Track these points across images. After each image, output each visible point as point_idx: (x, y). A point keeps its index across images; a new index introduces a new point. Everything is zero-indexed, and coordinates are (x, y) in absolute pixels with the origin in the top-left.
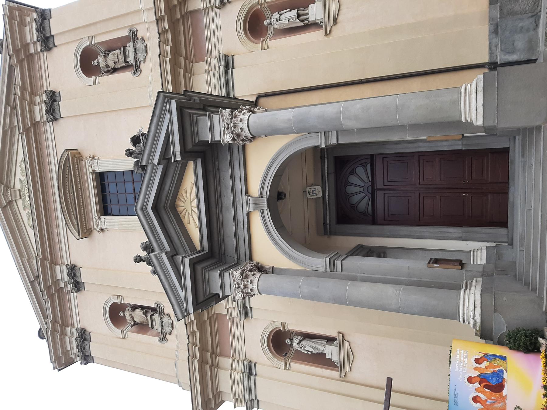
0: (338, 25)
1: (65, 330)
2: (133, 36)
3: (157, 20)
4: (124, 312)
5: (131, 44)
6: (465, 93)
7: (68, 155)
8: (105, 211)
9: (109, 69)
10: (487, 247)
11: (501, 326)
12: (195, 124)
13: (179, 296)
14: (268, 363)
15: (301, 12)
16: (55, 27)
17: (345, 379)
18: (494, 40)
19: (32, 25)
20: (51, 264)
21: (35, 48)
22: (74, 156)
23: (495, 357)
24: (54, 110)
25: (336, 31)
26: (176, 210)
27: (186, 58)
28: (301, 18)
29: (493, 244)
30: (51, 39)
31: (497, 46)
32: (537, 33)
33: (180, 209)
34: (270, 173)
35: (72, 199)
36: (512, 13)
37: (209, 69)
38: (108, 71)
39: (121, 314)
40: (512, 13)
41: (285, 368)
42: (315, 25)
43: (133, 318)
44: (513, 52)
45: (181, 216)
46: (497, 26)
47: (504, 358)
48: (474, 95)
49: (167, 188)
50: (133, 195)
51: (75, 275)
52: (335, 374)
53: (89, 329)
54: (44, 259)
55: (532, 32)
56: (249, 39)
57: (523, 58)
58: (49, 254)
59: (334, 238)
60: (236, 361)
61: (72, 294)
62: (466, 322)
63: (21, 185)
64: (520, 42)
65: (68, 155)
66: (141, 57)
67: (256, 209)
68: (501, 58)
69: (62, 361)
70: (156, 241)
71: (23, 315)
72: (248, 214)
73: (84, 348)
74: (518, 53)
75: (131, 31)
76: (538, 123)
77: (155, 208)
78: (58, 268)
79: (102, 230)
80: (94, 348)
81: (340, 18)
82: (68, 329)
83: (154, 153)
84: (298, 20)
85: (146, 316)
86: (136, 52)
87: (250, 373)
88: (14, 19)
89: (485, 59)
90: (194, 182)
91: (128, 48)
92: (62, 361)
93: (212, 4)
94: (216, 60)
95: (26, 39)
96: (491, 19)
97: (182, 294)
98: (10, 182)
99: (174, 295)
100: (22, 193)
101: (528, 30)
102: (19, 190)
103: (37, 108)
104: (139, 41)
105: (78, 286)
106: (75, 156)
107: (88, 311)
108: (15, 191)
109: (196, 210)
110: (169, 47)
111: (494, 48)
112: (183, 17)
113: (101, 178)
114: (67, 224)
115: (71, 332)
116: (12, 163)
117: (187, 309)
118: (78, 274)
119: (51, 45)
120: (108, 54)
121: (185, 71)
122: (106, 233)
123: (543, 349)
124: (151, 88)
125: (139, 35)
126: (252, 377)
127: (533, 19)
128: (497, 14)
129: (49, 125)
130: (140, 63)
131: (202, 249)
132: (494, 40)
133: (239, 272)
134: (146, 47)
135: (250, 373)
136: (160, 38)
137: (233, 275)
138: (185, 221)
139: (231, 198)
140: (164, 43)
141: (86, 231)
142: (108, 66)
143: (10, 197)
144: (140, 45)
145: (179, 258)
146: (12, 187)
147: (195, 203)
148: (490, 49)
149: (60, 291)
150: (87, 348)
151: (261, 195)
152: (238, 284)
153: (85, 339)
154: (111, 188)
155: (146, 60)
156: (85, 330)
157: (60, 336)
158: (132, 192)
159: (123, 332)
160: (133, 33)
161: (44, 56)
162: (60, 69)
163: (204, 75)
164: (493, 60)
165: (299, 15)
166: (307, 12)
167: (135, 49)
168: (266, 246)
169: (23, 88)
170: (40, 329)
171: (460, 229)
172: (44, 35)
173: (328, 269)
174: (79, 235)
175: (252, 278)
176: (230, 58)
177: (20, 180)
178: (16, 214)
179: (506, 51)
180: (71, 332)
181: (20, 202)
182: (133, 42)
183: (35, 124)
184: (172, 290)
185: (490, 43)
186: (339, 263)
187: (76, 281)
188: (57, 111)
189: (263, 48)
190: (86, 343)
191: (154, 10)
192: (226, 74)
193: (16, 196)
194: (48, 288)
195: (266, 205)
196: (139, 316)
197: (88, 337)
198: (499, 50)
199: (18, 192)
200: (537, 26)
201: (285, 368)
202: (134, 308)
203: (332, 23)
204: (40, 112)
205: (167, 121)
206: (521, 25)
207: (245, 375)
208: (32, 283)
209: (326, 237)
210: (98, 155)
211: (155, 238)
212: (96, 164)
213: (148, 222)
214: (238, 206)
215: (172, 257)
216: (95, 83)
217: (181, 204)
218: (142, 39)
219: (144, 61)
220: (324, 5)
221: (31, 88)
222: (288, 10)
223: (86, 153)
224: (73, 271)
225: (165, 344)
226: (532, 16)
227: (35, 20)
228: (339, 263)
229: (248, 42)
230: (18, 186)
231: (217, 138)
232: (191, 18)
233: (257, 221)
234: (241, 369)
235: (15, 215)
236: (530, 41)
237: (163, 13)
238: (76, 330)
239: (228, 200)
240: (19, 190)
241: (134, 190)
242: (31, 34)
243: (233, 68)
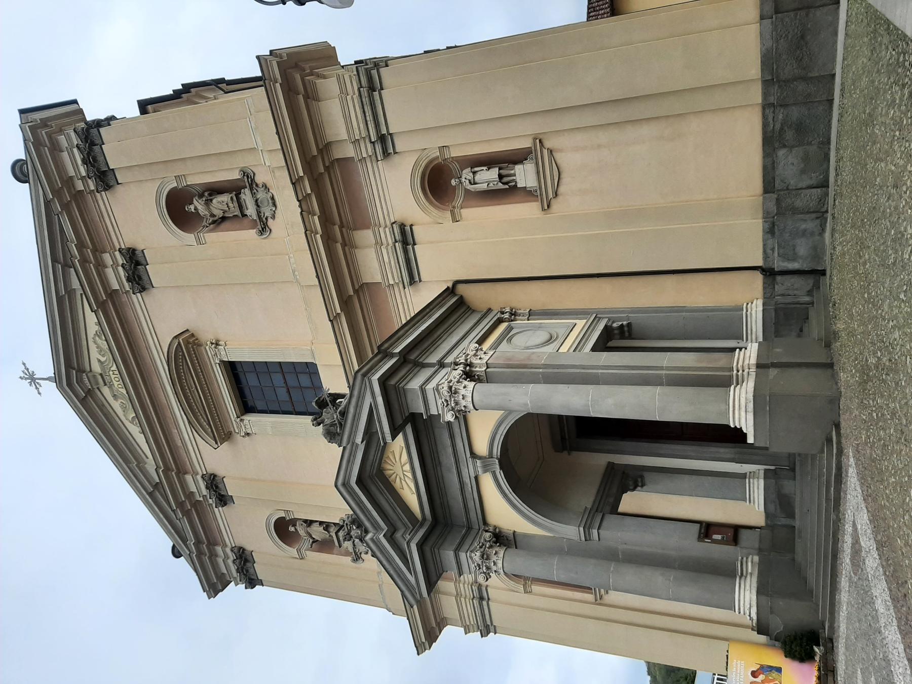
0: (560, 198)
1: (214, 550)
2: (248, 181)
3: (293, 184)
4: (294, 525)
5: (247, 191)
6: (734, 407)
7: (179, 343)
8: (246, 408)
9: (216, 218)
10: (766, 471)
11: (777, 624)
12: (403, 396)
13: (408, 580)
14: (502, 585)
15: (503, 172)
16: (114, 153)
17: (602, 602)
18: (769, 246)
19: (72, 152)
20: (178, 474)
21: (86, 184)
22: (187, 343)
23: (771, 668)
24: (140, 278)
25: (556, 205)
26: (383, 474)
27: (341, 226)
28: (505, 180)
29: (773, 468)
30: (110, 176)
31: (773, 249)
32: (824, 239)
33: (388, 473)
34: (500, 432)
35: (201, 408)
36: (795, 211)
37: (379, 243)
38: (214, 222)
39: (292, 529)
40: (795, 211)
41: (526, 592)
42: (528, 194)
43: (311, 536)
44: (794, 258)
45: (390, 479)
46: (773, 224)
47: (779, 670)
48: (743, 414)
49: (371, 457)
50: (285, 390)
51: (217, 487)
52: (590, 597)
53: (249, 547)
54: (167, 470)
55: (817, 238)
56: (431, 203)
57: (806, 266)
58: (174, 464)
59: (575, 453)
60: (461, 585)
61: (216, 510)
62: (742, 612)
63: (103, 368)
64: (803, 248)
65: (179, 343)
66: (267, 211)
67: (485, 472)
68: (779, 264)
69: (214, 585)
70: (369, 520)
71: (143, 532)
72: (476, 478)
73: (247, 571)
74: (801, 261)
75: (245, 173)
76: (813, 452)
77: (359, 481)
78: (189, 478)
79: (248, 434)
80: (260, 570)
81: (562, 189)
82: (219, 549)
83: (356, 432)
84: (500, 184)
85: (329, 532)
86: (258, 206)
87: (481, 598)
88: (41, 144)
89: (759, 262)
90: (403, 445)
91: (242, 196)
92: (214, 585)
93: (370, 154)
94: (387, 229)
95: (65, 171)
96: (766, 216)
97: (412, 579)
98: (83, 364)
99: (402, 580)
100: (107, 379)
101: (812, 234)
102: (101, 374)
103: (110, 272)
104: (261, 190)
105: (223, 500)
106: (189, 343)
107: (244, 525)
108: (94, 376)
109: (410, 475)
110: (316, 218)
111: (769, 252)
112: (327, 168)
113: (233, 369)
114: (189, 422)
115: (224, 552)
116: (80, 339)
117: (421, 595)
118: (220, 486)
119: (112, 182)
120: (211, 200)
121: (344, 245)
122: (253, 436)
123: (817, 658)
124: (292, 260)
125: (259, 179)
126: (485, 603)
127: (818, 221)
128: (773, 209)
129: (136, 298)
130: (266, 219)
131: (424, 518)
132: (770, 242)
133: (478, 554)
134: (273, 198)
135: (481, 598)
136: (300, 206)
137: (471, 558)
138: (397, 485)
139: (453, 460)
140: (309, 213)
141: (222, 434)
142: (213, 215)
143: (88, 384)
144: (261, 195)
145: (398, 535)
146: (88, 370)
147: (407, 467)
148: (765, 252)
149: (196, 505)
150: (251, 571)
151: (491, 455)
152: (479, 565)
153: (246, 561)
154: (251, 380)
155: (276, 215)
156: (244, 550)
157: (210, 558)
158: (288, 399)
159: (299, 551)
160: (248, 177)
161: (103, 198)
162: (133, 215)
163: (373, 250)
164: (770, 265)
165: (501, 177)
166: (512, 172)
167: (257, 201)
168: (502, 509)
169: (81, 246)
170: (174, 547)
171: (733, 450)
172: (98, 170)
173: (583, 539)
174: (216, 443)
175: (494, 558)
176: (408, 228)
177: (99, 361)
178: (103, 405)
179: (784, 257)
180: (224, 552)
181: (106, 391)
182: (251, 189)
183: (113, 295)
184: (399, 576)
185: (764, 245)
186: (595, 532)
187: (220, 494)
188: (145, 277)
189: (455, 220)
190: (249, 565)
191: (286, 168)
192: (406, 252)
193: (97, 383)
194: (180, 505)
195: (498, 467)
196: (318, 532)
197: (250, 558)
198: (776, 254)
199: (99, 377)
200: (823, 230)
201: (526, 592)
202: (309, 523)
203: (551, 195)
204: (116, 277)
205: (368, 400)
206: (803, 226)
207: (476, 602)
208: (151, 494)
209: (565, 453)
210: (222, 337)
211: (366, 516)
212: (223, 353)
213: (354, 499)
214: (462, 467)
215: (390, 537)
216: (199, 242)
217: (389, 467)
218: (265, 186)
219: (273, 217)
220: (538, 172)
221: (94, 243)
222: (485, 168)
223: (206, 335)
224: (213, 483)
225: (360, 564)
226: (817, 218)
227: (77, 146)
228: (595, 532)
229: (431, 208)
230: (97, 368)
231: (434, 411)
232: (339, 166)
233: (487, 482)
234: (469, 594)
235: (102, 407)
236: (815, 248)
237: (301, 174)
238: (232, 551)
239: (447, 459)
240: (101, 374)
241: (286, 382)
242: (74, 164)
243: (414, 244)
